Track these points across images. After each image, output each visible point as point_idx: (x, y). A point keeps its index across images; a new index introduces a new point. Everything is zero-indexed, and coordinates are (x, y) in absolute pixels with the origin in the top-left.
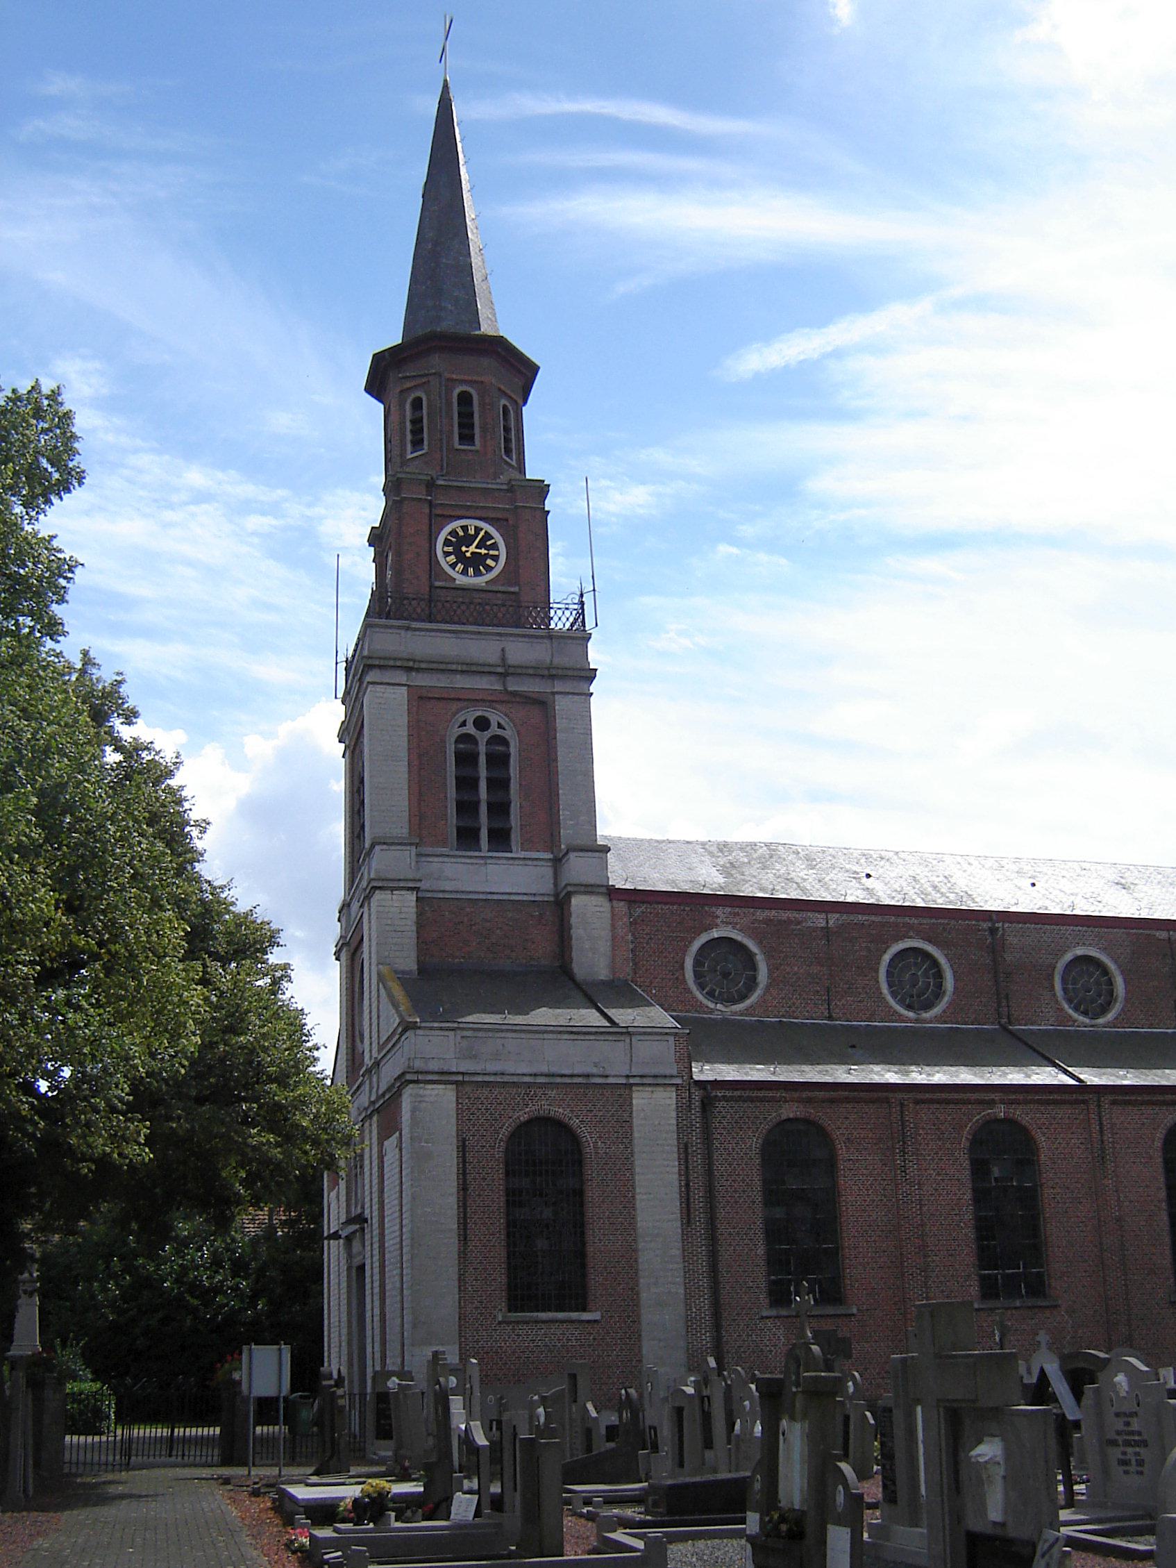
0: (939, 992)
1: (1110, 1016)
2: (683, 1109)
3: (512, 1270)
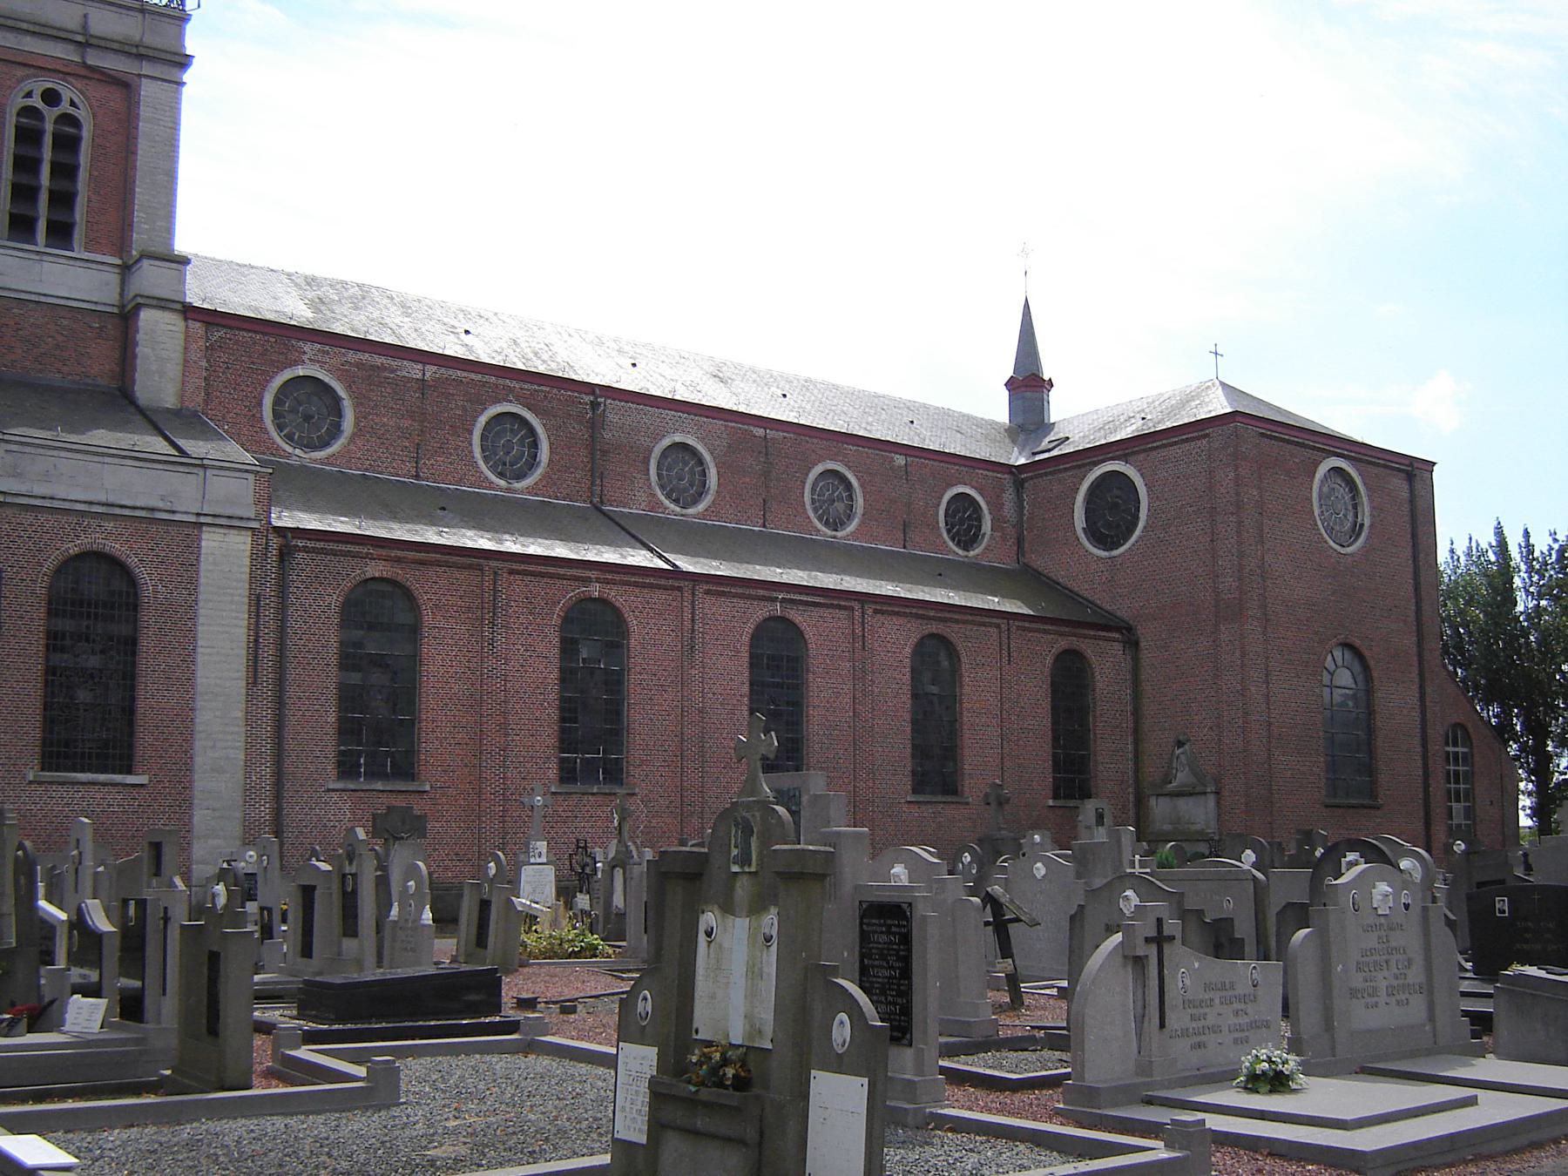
0: (533, 463)
1: (701, 507)
2: (258, 556)
3: (49, 723)
